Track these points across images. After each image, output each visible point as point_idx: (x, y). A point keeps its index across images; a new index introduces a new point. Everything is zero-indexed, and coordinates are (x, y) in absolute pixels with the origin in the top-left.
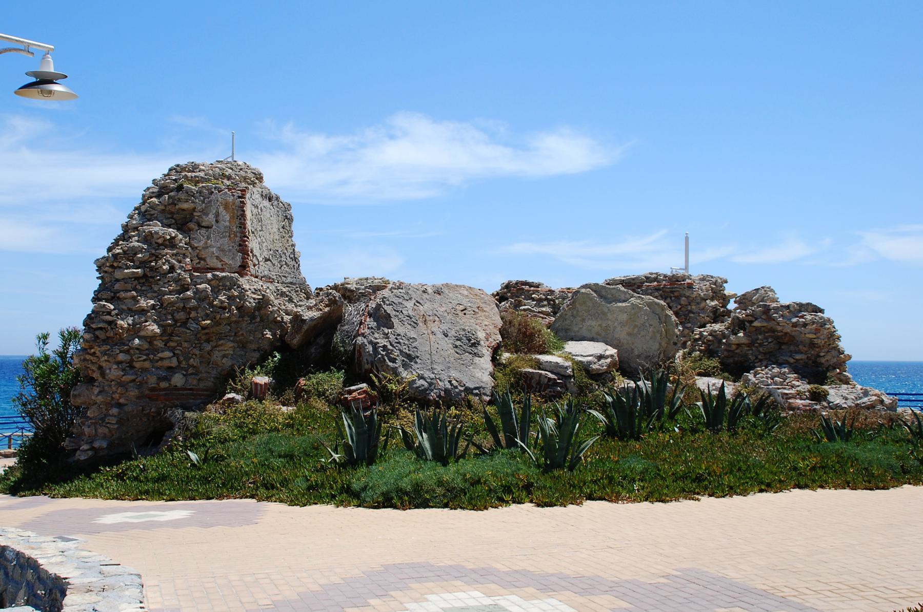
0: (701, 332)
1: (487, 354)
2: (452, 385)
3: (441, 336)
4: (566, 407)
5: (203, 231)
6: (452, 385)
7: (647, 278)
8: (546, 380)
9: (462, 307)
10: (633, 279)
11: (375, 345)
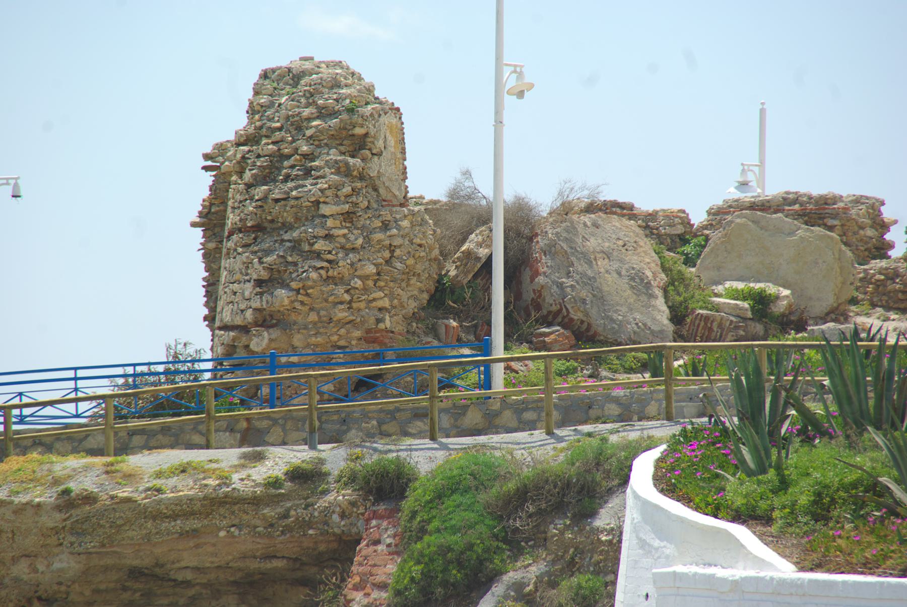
0: (865, 270)
1: (659, 293)
2: (639, 327)
3: (615, 275)
4: (37, 500)
5: (376, 158)
6: (639, 327)
7: (785, 199)
8: (728, 323)
9: (621, 243)
10: (768, 201)
11: (561, 286)
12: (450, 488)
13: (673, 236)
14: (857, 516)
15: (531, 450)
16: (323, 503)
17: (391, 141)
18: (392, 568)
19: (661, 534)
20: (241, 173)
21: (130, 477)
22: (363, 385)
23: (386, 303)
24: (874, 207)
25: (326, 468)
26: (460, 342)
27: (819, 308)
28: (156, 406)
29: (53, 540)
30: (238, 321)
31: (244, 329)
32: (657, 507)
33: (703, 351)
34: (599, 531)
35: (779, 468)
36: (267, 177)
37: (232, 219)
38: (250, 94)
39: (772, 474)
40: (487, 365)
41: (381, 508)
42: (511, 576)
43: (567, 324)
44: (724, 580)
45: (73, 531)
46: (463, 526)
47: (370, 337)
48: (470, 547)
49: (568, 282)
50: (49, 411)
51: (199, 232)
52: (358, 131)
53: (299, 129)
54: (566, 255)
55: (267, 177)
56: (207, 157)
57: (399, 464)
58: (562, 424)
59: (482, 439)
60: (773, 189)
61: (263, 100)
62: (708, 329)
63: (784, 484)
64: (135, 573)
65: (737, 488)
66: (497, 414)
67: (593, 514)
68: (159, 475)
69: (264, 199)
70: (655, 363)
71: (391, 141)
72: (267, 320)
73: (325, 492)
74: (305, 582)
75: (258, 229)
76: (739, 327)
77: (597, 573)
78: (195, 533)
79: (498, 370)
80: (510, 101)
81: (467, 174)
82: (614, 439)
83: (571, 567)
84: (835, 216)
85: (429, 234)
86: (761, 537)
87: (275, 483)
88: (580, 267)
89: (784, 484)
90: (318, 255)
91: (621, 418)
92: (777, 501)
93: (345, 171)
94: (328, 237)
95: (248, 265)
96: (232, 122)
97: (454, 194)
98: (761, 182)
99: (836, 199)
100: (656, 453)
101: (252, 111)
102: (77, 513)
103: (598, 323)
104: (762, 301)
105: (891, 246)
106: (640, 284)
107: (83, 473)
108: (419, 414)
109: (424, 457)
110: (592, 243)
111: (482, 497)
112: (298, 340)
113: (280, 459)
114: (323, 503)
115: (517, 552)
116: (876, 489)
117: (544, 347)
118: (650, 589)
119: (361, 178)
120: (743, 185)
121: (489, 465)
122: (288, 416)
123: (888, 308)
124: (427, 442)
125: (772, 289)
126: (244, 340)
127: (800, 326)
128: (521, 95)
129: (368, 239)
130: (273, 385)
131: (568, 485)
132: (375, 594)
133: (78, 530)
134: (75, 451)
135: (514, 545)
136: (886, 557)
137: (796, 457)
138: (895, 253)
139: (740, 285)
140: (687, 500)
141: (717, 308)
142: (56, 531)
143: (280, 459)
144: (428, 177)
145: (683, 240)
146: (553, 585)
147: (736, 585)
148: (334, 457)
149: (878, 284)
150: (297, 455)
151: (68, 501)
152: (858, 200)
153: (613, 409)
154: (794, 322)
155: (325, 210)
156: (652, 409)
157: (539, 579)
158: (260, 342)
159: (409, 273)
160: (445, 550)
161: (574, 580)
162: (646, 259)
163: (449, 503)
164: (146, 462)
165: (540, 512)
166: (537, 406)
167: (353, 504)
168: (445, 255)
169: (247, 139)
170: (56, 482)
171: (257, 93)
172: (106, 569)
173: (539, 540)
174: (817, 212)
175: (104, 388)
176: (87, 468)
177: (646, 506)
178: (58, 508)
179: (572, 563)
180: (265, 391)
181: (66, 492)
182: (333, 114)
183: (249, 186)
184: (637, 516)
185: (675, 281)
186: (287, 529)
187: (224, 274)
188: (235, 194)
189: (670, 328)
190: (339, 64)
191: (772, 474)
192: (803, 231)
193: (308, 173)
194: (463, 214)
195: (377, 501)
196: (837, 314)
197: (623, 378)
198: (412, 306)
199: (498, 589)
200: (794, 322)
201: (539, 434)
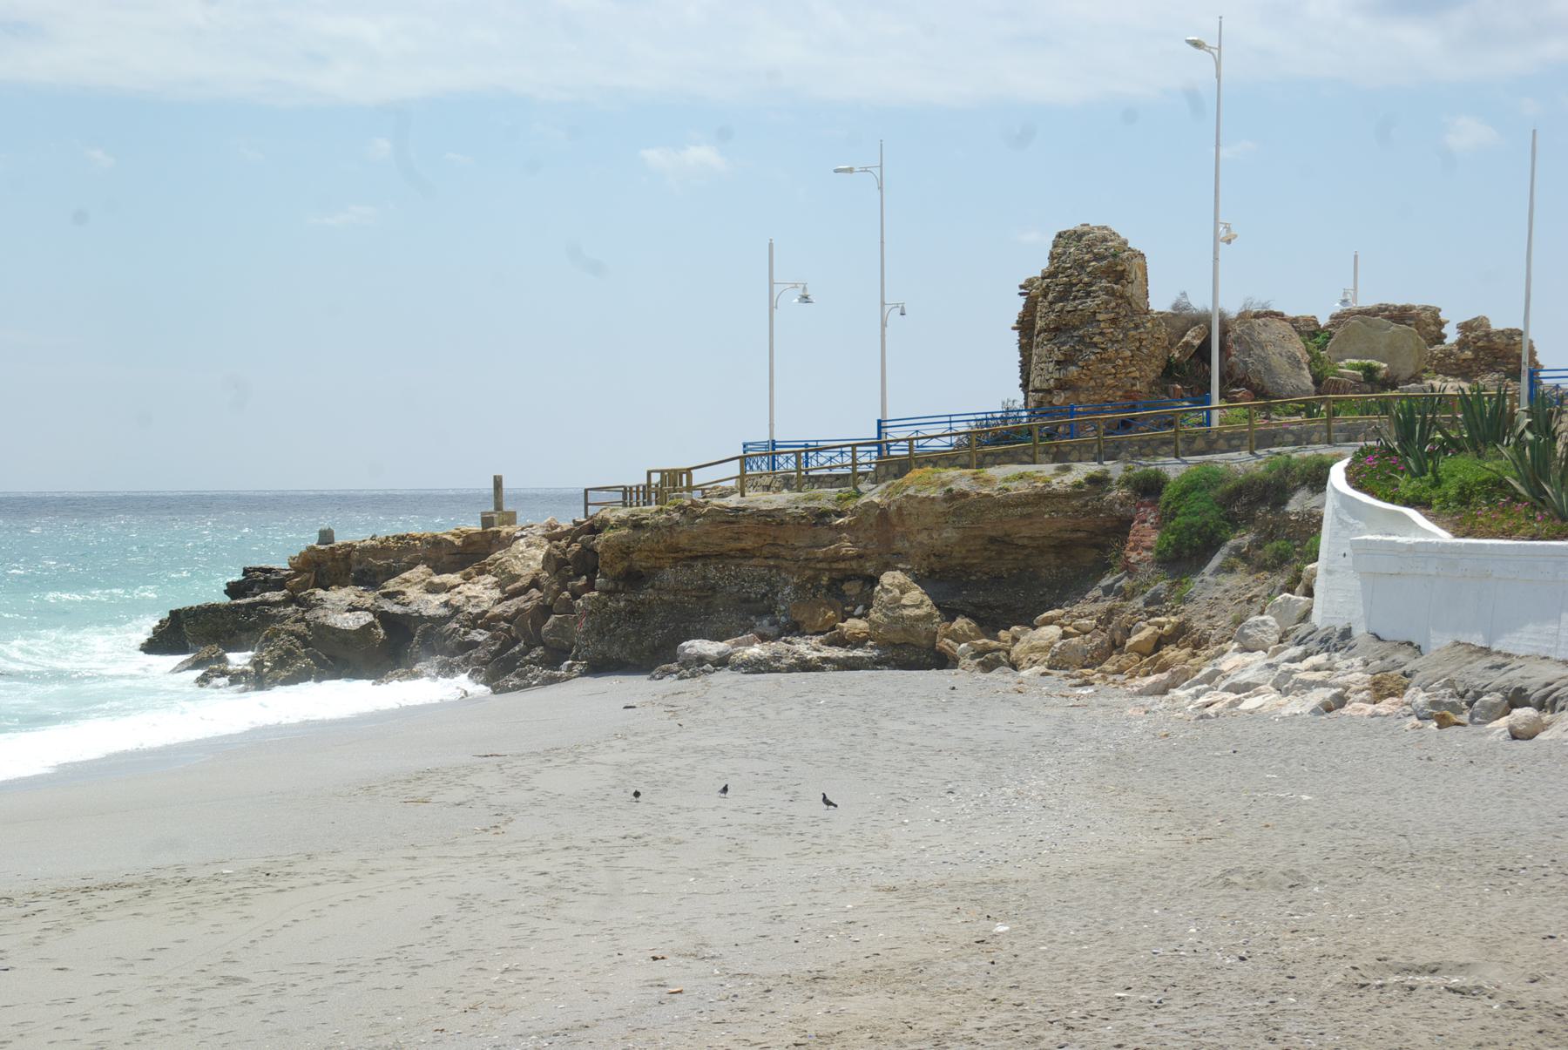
11: (1245, 363)
12: (1190, 487)
13: (1308, 330)
14: (1490, 502)
15: (1241, 463)
16: (1109, 497)
17: (1139, 274)
18: (1155, 537)
19: (1355, 515)
20: (1045, 296)
21: (988, 481)
22: (1125, 425)
23: (1137, 374)
24: (1435, 312)
25: (1110, 475)
26: (1183, 398)
27: (1405, 375)
28: (993, 440)
29: (942, 520)
30: (1045, 386)
31: (1049, 391)
32: (1352, 498)
33: (1335, 401)
34: (1289, 514)
35: (1434, 472)
36: (1063, 297)
37: (1040, 324)
38: (1050, 247)
39: (1429, 475)
40: (1209, 411)
41: (1146, 500)
42: (1232, 542)
43: (1249, 386)
44: (1402, 544)
45: (954, 514)
46: (1201, 511)
47: (1128, 395)
48: (1206, 524)
49: (1250, 360)
50: (934, 442)
51: (1016, 333)
52: (1120, 268)
53: (1082, 267)
54: (1247, 343)
55: (1063, 297)
56: (1021, 287)
57: (1157, 473)
58: (1258, 447)
59: (1208, 457)
60: (1367, 301)
61: (1060, 250)
62: (1336, 387)
63: (1437, 483)
64: (992, 540)
65: (1405, 484)
66: (1215, 441)
67: (1285, 503)
68: (1006, 480)
69: (1061, 311)
70: (1308, 409)
71: (1139, 274)
72: (1062, 385)
73: (1110, 491)
74: (1096, 546)
75: (1057, 330)
76: (1357, 386)
77: (1288, 540)
78: (1029, 516)
79: (1216, 414)
80: (1222, 245)
81: (1184, 294)
82: (1294, 456)
83: (1271, 537)
84: (1411, 318)
85: (1163, 332)
86: (1425, 516)
87: (1078, 485)
88: (1257, 351)
89: (1437, 483)
90: (1095, 345)
91: (1295, 444)
92: (1434, 493)
93: (1111, 293)
94: (1101, 334)
95: (1051, 352)
96: (1038, 265)
97: (1175, 307)
98: (1355, 300)
99: (1412, 308)
100: (1345, 463)
101: (1052, 257)
102: (957, 504)
103: (1268, 385)
104: (1370, 371)
105: (1445, 336)
106: (1295, 362)
107: (960, 479)
108: (1166, 442)
109: (1173, 469)
110: (1264, 336)
111: (1212, 493)
112: (1082, 398)
113: (1082, 471)
114: (1109, 497)
115: (1236, 528)
116: (1501, 485)
117: (1236, 400)
118: (1347, 550)
119: (1122, 297)
120: (1344, 302)
121: (1216, 473)
122: (1081, 444)
123: (1446, 375)
124: (1173, 460)
125: (1376, 363)
126: (1049, 398)
127: (1394, 387)
128: (1229, 242)
129: (1126, 335)
130: (1071, 425)
131: (1268, 485)
132: (1144, 554)
133: (957, 513)
134: (951, 466)
135: (1234, 523)
136: (1519, 528)
137: (1446, 464)
138: (1447, 341)
139: (1356, 362)
140: (1372, 494)
141: (1342, 375)
142: (944, 514)
143: (1082, 471)
144: (1160, 300)
145: (1314, 335)
146: (1260, 547)
147: (1411, 548)
148: (1115, 469)
149: (1440, 359)
150: (1092, 468)
151: (951, 496)
152: (1425, 309)
153: (1290, 438)
154: (1390, 383)
155: (1100, 317)
156: (1315, 437)
157: (1251, 544)
158: (1059, 399)
159: (1152, 355)
160: (1189, 526)
161: (1275, 544)
162: (1297, 346)
163: (1191, 496)
164: (998, 473)
165: (1250, 503)
166: (1241, 436)
167: (1128, 498)
168: (1172, 344)
169: (1050, 275)
170: (943, 484)
171: (1055, 246)
172: (975, 537)
173: (1249, 520)
174: (1401, 315)
175: (962, 427)
176: (961, 476)
177: (1343, 496)
178: (945, 500)
179: (1271, 534)
180: (1061, 429)
181: (950, 490)
182: (1104, 258)
183: (1051, 303)
184: (1337, 504)
185: (1315, 360)
186: (1087, 514)
187: (1035, 358)
188: (1041, 308)
189: (1313, 388)
190: (1105, 228)
191: (1429, 475)
192: (1394, 327)
193: (1088, 294)
194: (1183, 320)
195: (1143, 496)
196: (1416, 378)
197: (1285, 419)
198: (1153, 375)
199: (1224, 550)
200: (1390, 383)
201: (1245, 454)
